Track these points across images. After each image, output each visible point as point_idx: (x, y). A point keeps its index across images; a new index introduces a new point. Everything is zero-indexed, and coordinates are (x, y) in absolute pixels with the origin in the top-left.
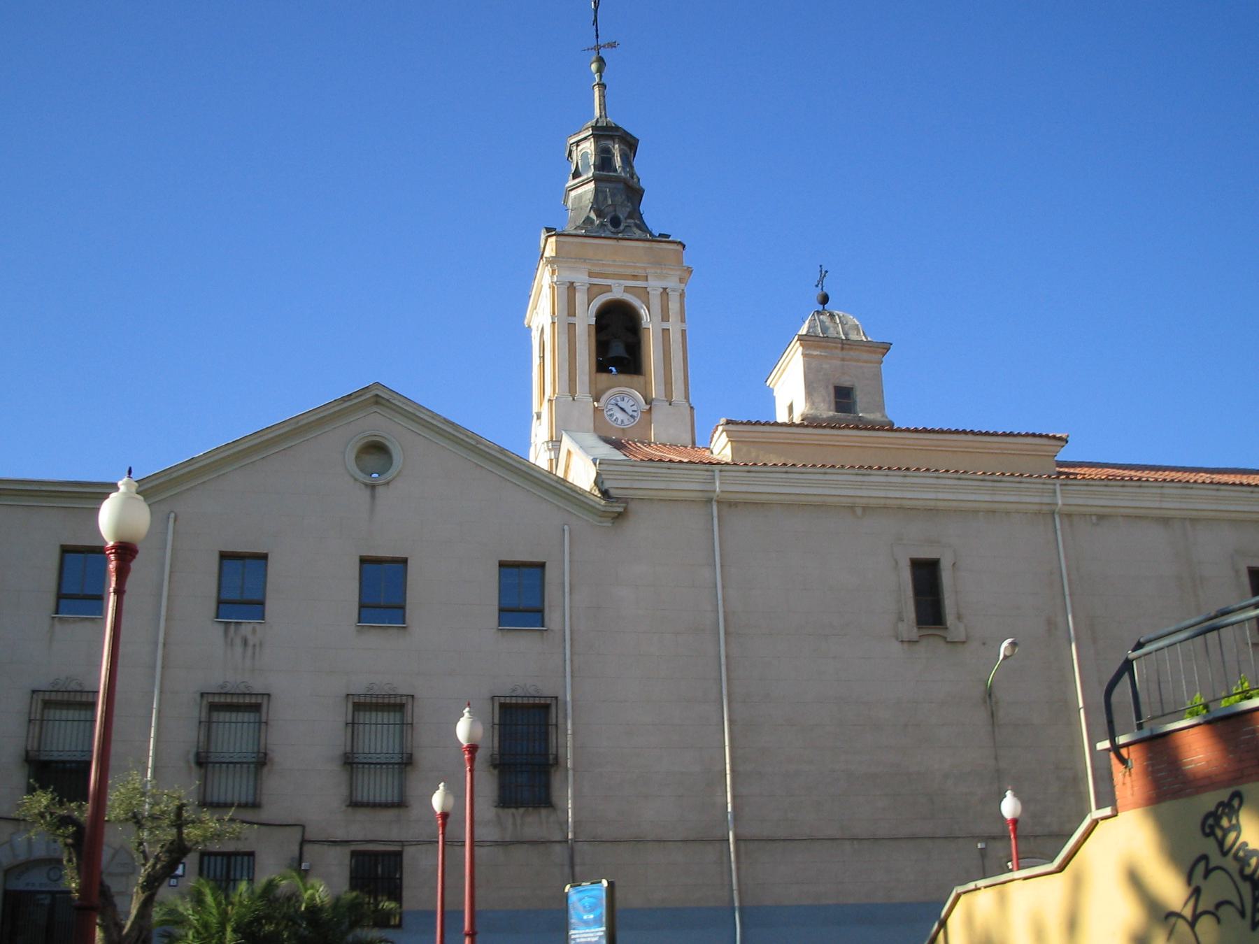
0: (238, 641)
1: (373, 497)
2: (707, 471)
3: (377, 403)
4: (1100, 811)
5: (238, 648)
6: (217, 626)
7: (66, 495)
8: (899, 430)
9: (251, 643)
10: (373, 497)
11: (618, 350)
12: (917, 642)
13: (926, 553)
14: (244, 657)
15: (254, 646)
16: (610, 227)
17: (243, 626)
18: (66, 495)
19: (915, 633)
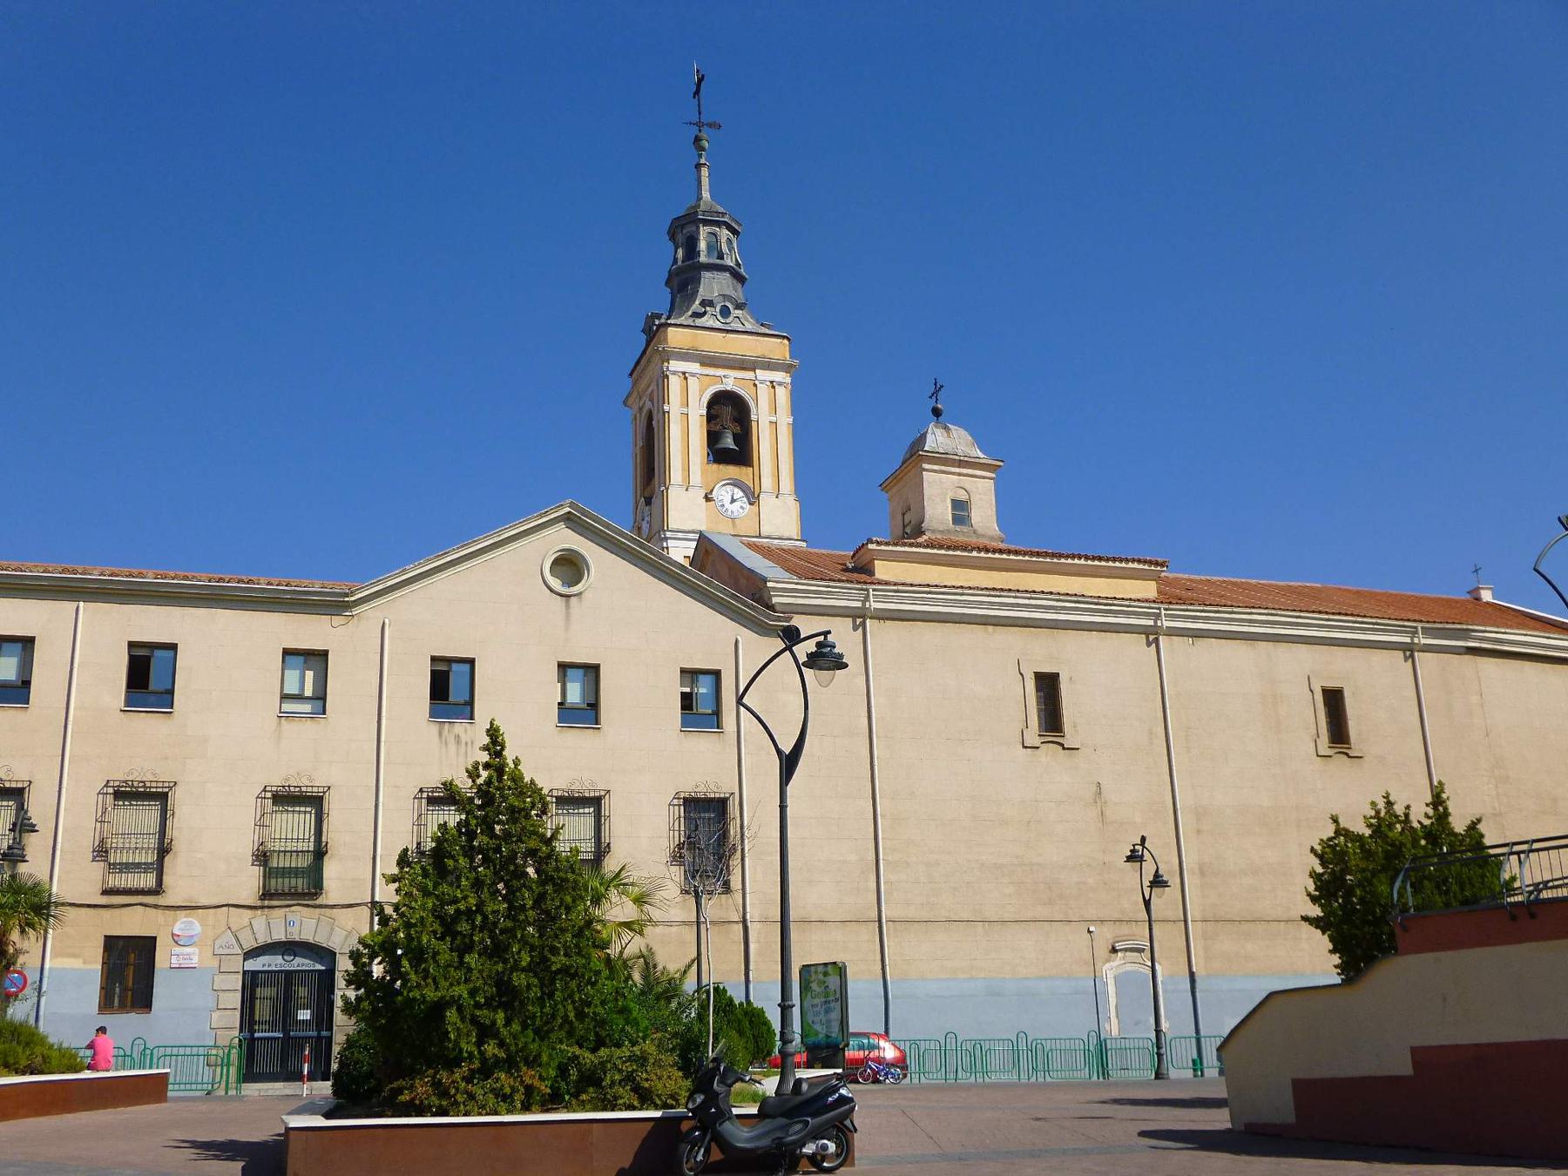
0: (452, 740)
1: (568, 606)
2: (862, 590)
3: (568, 519)
4: (698, 411)
5: (452, 747)
6: (432, 725)
7: (1281, 638)
8: (699, 954)
9: (463, 741)
10: (568, 606)
11: (729, 442)
12: (1038, 748)
13: (1332, 684)
14: (458, 755)
15: (466, 743)
16: (719, 317)
17: (457, 725)
18: (1281, 638)
19: (1037, 741)
